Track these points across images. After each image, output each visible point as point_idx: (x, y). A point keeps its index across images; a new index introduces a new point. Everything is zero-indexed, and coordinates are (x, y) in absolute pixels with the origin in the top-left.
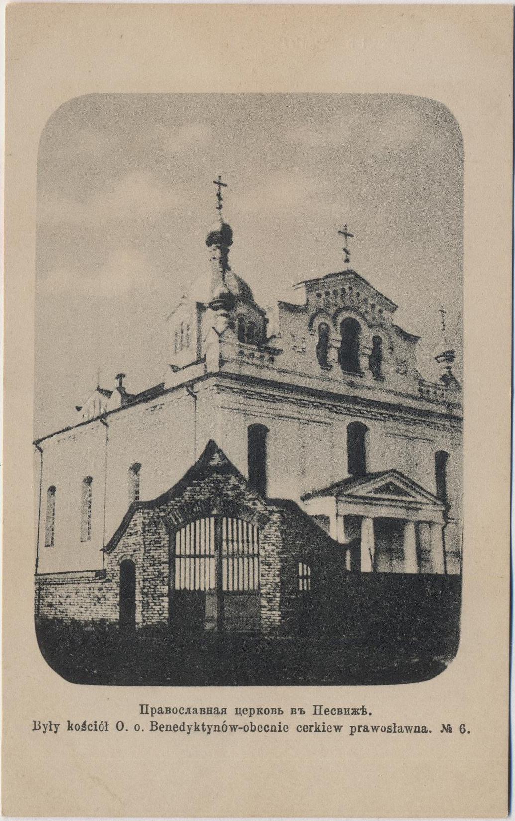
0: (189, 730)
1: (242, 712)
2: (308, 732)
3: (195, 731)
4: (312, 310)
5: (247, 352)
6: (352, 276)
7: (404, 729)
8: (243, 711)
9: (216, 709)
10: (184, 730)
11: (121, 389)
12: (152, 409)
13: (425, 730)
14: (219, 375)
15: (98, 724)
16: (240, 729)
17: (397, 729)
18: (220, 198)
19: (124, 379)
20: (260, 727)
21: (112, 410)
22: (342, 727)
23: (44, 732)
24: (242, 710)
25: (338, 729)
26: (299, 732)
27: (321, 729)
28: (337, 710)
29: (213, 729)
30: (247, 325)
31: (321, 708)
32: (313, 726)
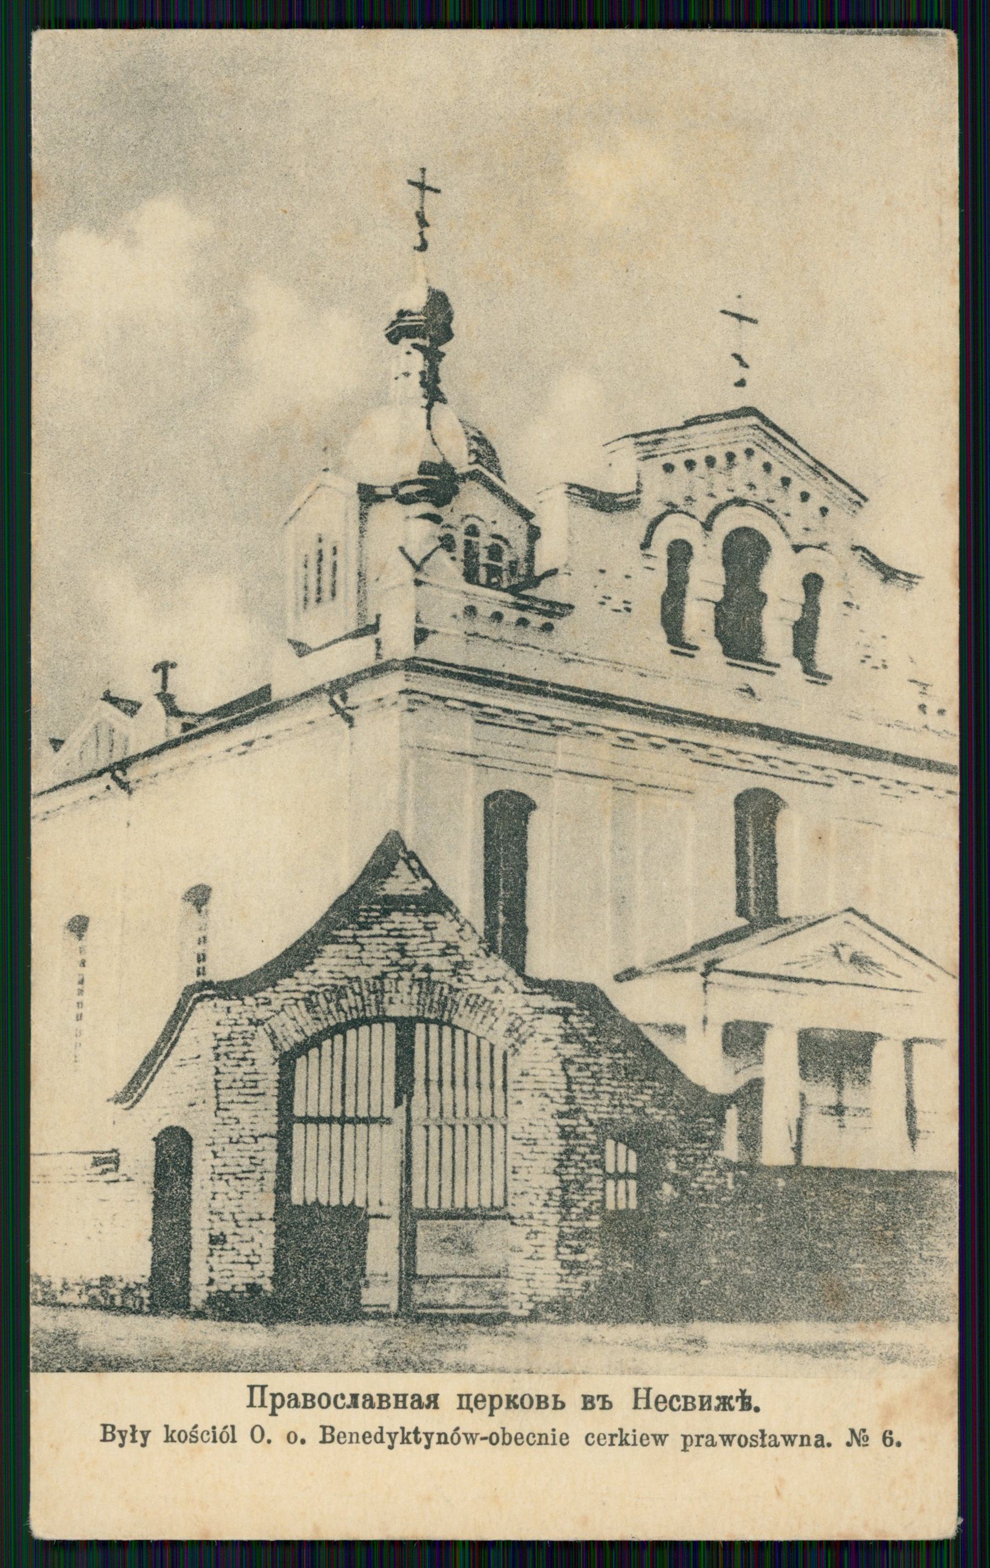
0: (393, 1441)
1: (472, 1405)
2: (606, 1446)
3: (402, 1443)
4: (651, 506)
5: (485, 610)
6: (754, 420)
7: (780, 1440)
8: (476, 1402)
9: (368, 1397)
10: (382, 1441)
11: (166, 698)
12: (243, 749)
13: (820, 1442)
14: (412, 665)
15: (218, 1431)
16: (482, 1439)
17: (767, 1440)
18: (423, 223)
19: (171, 672)
20: (519, 1436)
21: (143, 749)
22: (666, 1435)
23: (121, 1446)
24: (472, 1399)
25: (660, 1439)
26: (589, 1445)
27: (630, 1440)
28: (682, 1400)
29: (435, 1439)
30: (484, 541)
31: (648, 1394)
32: (616, 1435)
